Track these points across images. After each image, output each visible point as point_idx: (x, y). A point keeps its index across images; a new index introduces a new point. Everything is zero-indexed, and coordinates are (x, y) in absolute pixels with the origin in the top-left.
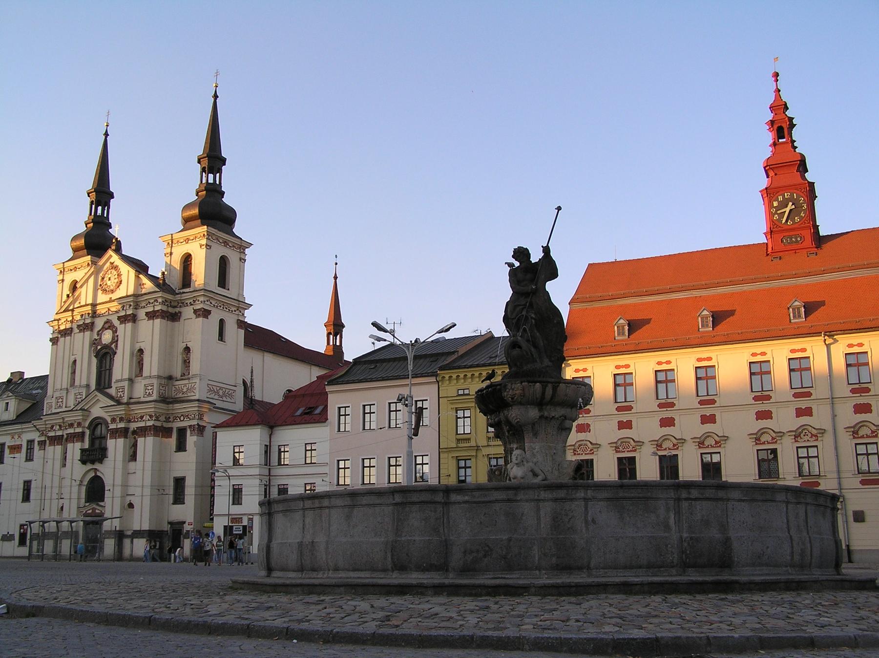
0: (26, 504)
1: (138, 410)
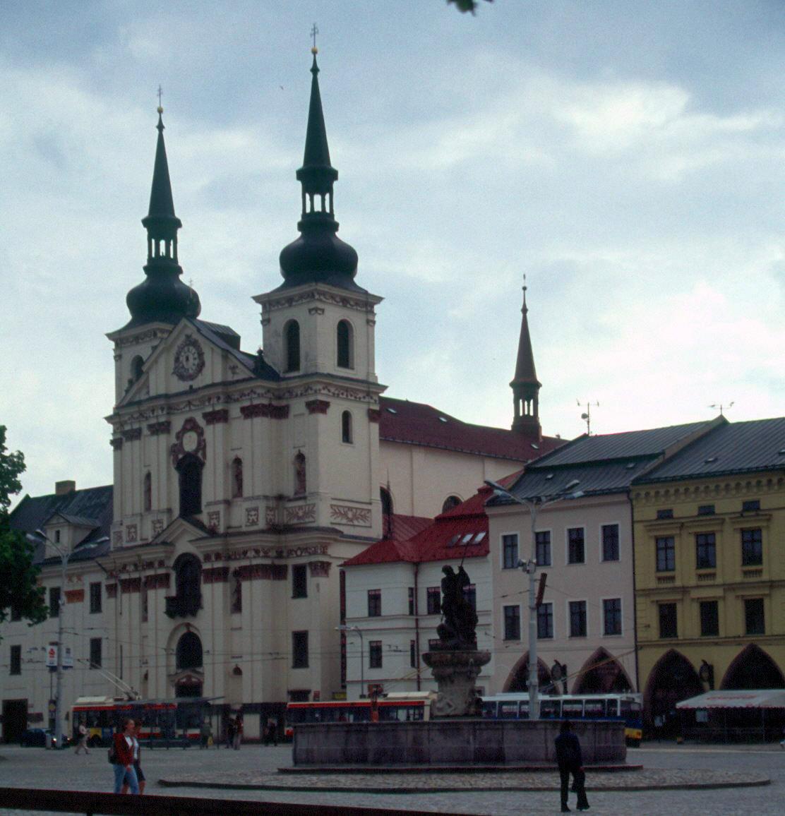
0: (577, 568)
1: (238, 544)
